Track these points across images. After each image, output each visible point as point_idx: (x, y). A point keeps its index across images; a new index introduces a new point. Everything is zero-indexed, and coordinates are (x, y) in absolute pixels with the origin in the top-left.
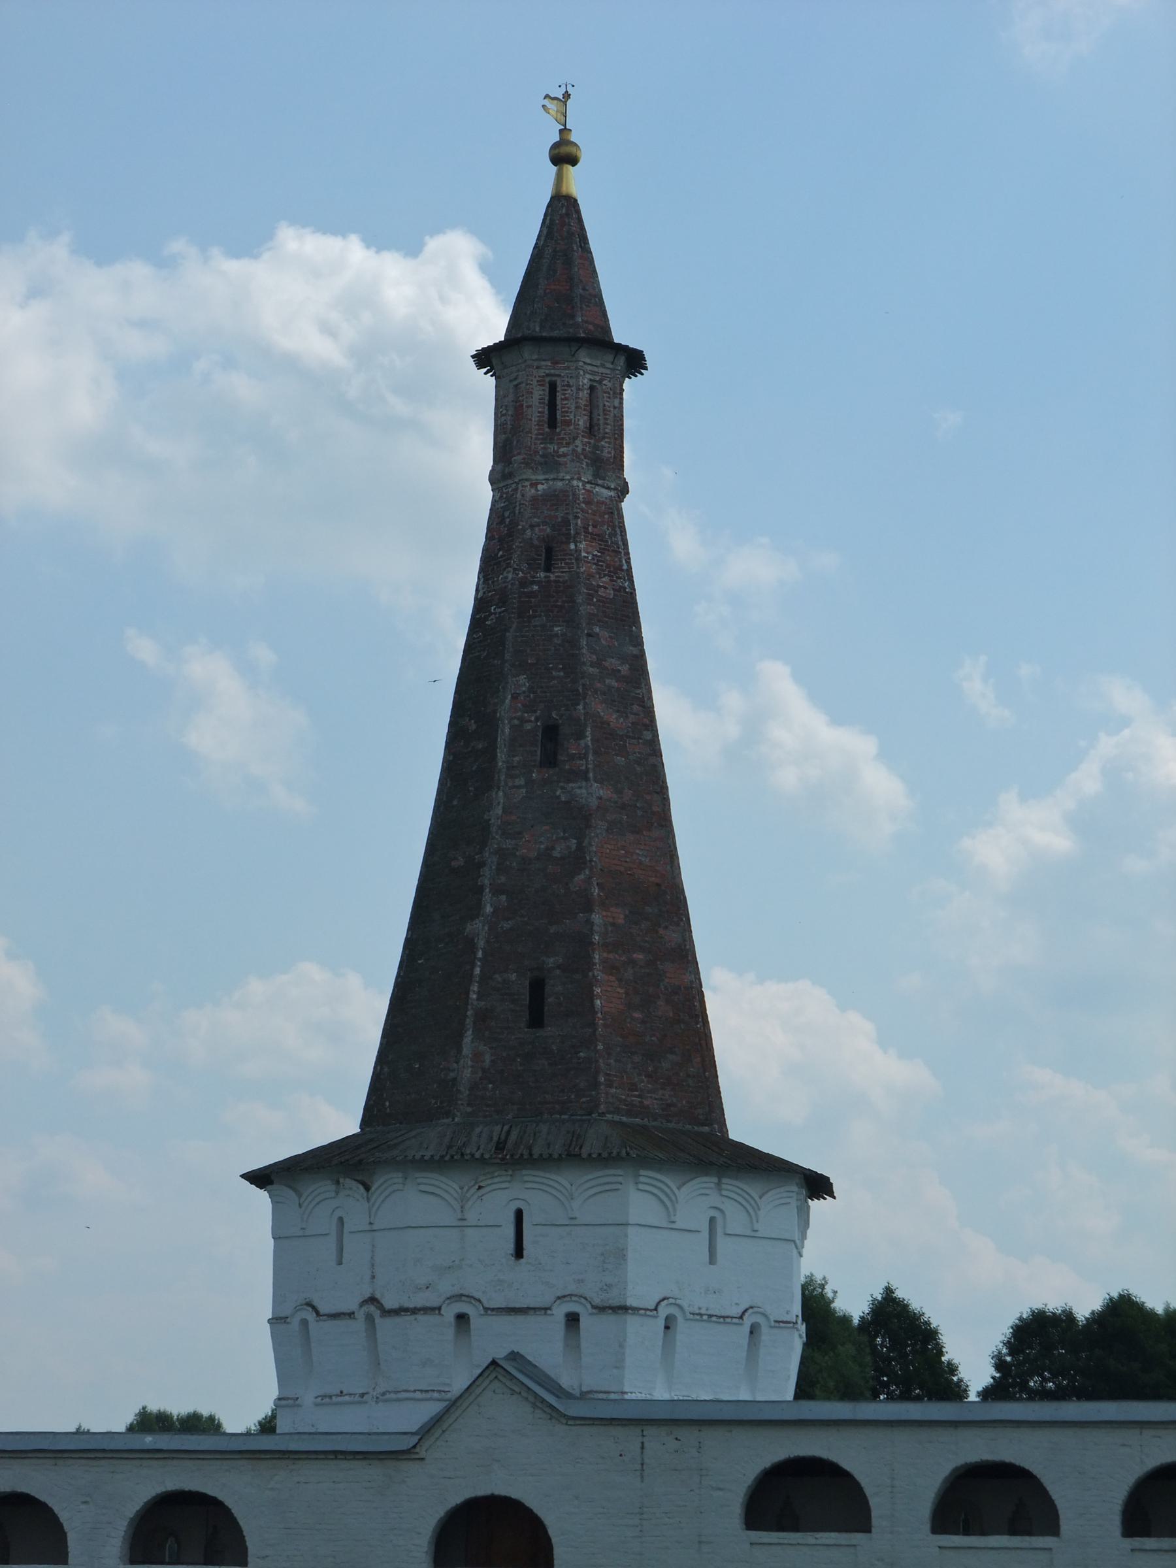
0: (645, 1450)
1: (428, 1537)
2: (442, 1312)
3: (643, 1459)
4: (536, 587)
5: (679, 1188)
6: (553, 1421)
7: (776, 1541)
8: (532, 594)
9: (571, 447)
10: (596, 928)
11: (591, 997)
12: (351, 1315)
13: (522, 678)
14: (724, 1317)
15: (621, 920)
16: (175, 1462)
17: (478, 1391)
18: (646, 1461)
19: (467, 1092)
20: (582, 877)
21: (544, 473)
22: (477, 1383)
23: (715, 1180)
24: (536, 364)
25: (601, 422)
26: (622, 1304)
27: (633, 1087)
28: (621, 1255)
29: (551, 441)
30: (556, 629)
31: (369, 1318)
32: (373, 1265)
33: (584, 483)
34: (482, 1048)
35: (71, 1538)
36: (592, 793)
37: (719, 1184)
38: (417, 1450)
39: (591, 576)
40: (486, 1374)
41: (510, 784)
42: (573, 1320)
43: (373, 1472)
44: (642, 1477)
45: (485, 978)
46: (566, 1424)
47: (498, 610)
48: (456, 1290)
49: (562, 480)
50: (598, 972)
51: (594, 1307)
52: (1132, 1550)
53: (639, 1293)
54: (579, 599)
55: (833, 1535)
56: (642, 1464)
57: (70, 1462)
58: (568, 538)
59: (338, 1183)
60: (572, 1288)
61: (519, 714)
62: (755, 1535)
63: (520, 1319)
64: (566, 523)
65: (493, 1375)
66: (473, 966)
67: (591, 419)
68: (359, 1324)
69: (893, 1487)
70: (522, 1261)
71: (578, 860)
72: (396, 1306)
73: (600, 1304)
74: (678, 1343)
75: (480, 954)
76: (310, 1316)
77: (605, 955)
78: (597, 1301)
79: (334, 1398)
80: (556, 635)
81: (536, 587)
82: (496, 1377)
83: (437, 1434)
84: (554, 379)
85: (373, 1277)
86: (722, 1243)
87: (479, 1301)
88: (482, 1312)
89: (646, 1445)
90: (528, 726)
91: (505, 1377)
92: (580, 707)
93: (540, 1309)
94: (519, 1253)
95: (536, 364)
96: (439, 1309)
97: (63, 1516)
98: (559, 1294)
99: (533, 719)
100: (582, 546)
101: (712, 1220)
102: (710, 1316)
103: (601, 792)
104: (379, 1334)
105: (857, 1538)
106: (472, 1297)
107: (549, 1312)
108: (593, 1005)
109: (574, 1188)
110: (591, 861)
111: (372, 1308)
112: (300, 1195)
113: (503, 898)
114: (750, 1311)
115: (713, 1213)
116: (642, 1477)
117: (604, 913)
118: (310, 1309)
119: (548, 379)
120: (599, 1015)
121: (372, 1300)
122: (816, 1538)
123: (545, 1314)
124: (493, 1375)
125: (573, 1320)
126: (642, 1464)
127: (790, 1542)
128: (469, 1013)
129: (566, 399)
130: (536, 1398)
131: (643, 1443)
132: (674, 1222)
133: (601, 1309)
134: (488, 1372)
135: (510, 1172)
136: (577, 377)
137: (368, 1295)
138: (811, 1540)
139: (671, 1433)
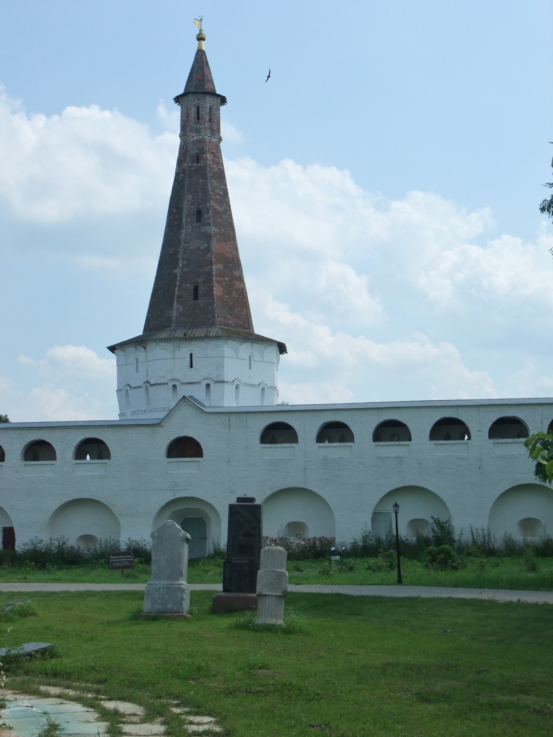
2: (169, 384)
4: (194, 168)
8: (193, 170)
11: (212, 290)
12: (141, 387)
13: (190, 196)
18: (231, 424)
20: (209, 255)
21: (196, 133)
22: (179, 403)
23: (251, 344)
27: (225, 318)
28: (222, 366)
31: (147, 388)
37: (252, 345)
38: (161, 423)
42: (208, 386)
44: (229, 429)
45: (180, 286)
47: (183, 175)
49: (201, 136)
56: (229, 426)
58: (204, 153)
60: (208, 376)
63: (192, 385)
64: (203, 148)
65: (184, 401)
66: (176, 282)
68: (143, 390)
71: (208, 250)
76: (128, 388)
77: (217, 278)
78: (215, 380)
81: (194, 168)
84: (199, 105)
86: (253, 363)
90: (192, 210)
92: (208, 204)
94: (191, 366)
96: (167, 383)
101: (250, 357)
102: (250, 384)
105: (294, 445)
106: (177, 380)
108: (213, 292)
110: (212, 250)
111: (147, 384)
112: (124, 352)
113: (185, 262)
120: (215, 296)
121: (147, 382)
124: (184, 401)
125: (208, 386)
126: (229, 426)
129: (202, 111)
131: (229, 419)
133: (217, 382)
134: (182, 400)
135: (188, 342)
136: (206, 104)
137: (146, 381)
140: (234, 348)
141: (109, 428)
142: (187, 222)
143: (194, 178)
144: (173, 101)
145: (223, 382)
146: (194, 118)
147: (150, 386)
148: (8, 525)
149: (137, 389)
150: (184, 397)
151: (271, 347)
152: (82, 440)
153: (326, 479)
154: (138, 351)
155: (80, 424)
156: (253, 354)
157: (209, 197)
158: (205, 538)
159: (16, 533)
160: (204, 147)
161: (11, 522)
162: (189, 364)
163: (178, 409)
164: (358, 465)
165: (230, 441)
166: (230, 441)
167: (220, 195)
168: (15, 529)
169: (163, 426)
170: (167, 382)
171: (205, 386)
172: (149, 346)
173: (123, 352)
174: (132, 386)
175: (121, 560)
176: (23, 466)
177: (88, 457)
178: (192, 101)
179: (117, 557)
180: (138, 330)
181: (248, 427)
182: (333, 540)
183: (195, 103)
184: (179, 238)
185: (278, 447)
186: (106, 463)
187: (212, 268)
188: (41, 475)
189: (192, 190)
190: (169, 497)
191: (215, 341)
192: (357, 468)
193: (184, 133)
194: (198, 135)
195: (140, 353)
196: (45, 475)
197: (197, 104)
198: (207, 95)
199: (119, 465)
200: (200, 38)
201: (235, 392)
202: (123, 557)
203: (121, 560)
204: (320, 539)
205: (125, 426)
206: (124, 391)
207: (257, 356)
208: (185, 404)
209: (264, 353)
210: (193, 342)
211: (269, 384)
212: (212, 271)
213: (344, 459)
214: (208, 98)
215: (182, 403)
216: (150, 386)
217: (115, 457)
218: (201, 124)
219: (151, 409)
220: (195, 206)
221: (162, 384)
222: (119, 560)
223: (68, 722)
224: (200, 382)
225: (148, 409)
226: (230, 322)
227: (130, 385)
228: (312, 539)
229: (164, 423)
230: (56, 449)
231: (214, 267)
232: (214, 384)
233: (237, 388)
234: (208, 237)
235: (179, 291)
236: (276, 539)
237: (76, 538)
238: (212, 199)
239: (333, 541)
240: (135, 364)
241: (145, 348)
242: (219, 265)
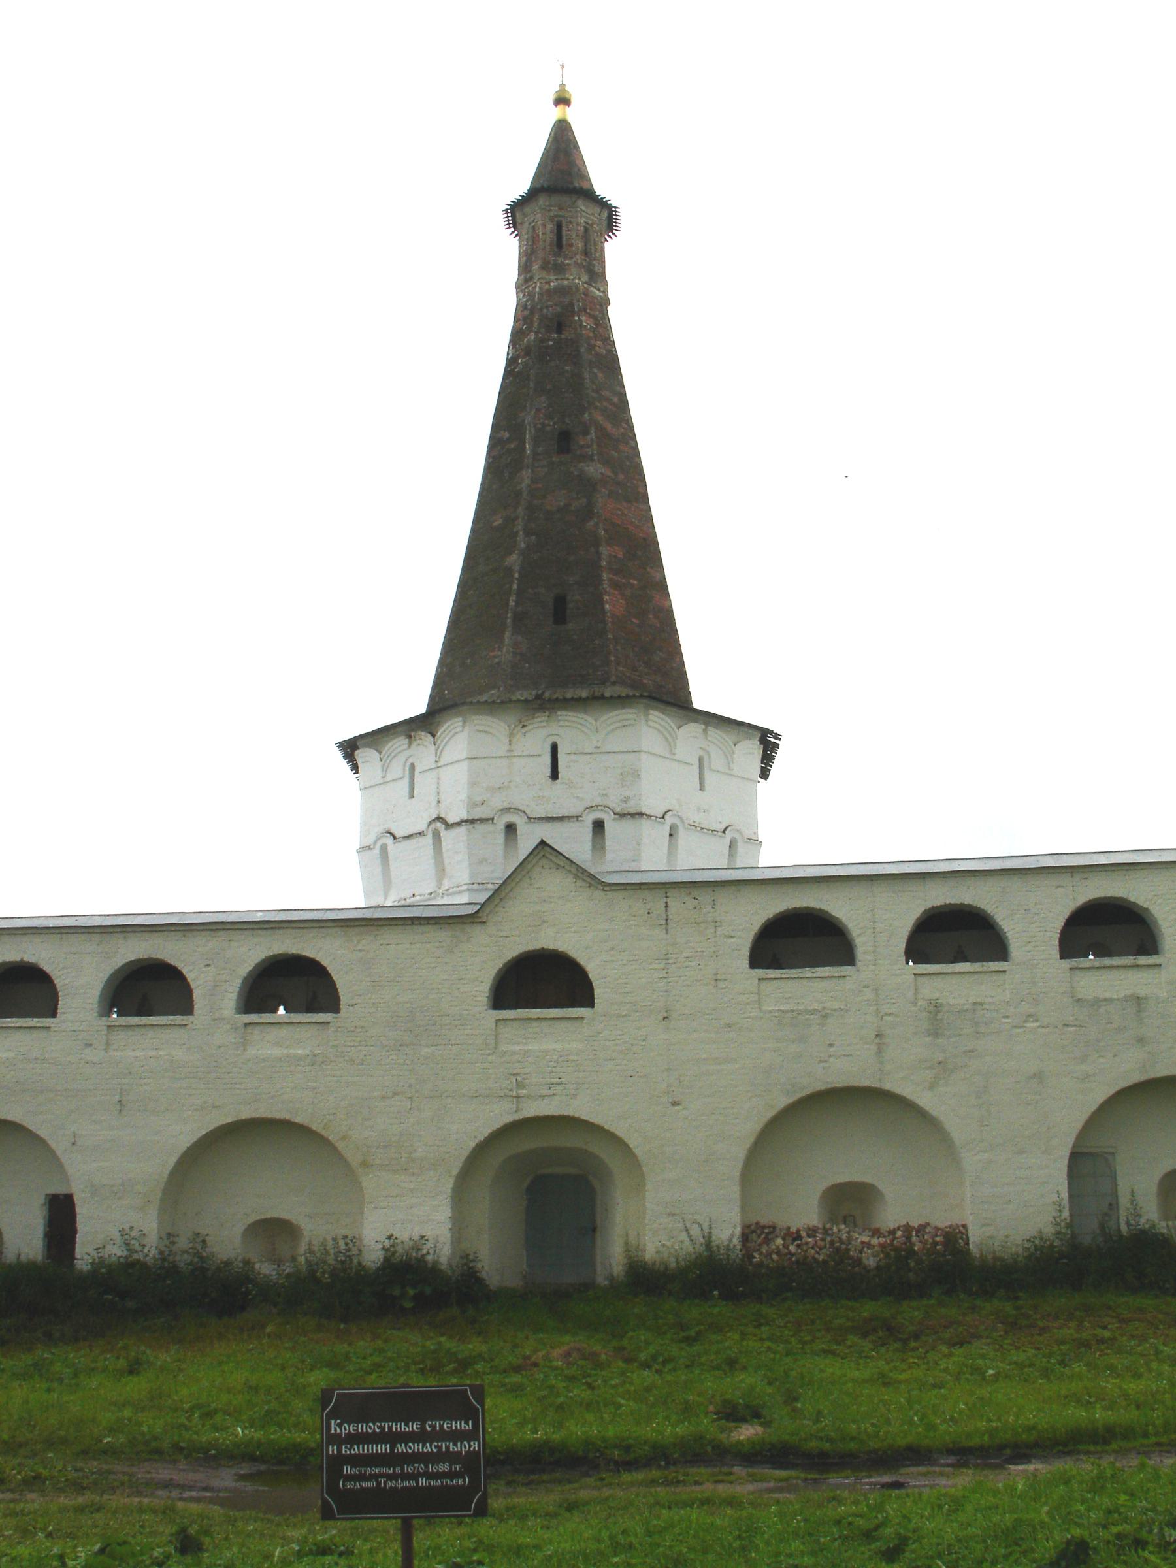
0: (668, 909)
1: (489, 985)
2: (495, 821)
3: (667, 916)
4: (551, 343)
5: (679, 728)
6: (592, 888)
7: (779, 976)
8: (547, 347)
9: (574, 259)
10: (604, 556)
11: (602, 603)
12: (421, 834)
13: (543, 399)
14: (712, 831)
15: (620, 555)
16: (281, 932)
17: (529, 866)
18: (670, 917)
19: (510, 670)
20: (592, 523)
22: (529, 859)
23: (703, 727)
24: (548, 208)
25: (593, 251)
26: (639, 811)
27: (634, 669)
28: (636, 774)
29: (559, 256)
30: (567, 368)
31: (437, 836)
32: (438, 793)
33: (583, 283)
34: (520, 638)
35: (197, 994)
36: (594, 470)
37: (705, 730)
38: (480, 915)
39: (589, 338)
40: (535, 853)
41: (536, 465)
42: (599, 826)
43: (442, 935)
44: (667, 930)
45: (520, 592)
46: (603, 890)
47: (524, 360)
48: (506, 805)
49: (568, 279)
50: (605, 585)
51: (615, 814)
52: (1071, 969)
53: (652, 803)
54: (582, 350)
55: (827, 968)
56: (667, 920)
57: (195, 933)
58: (573, 314)
59: (410, 737)
60: (598, 801)
61: (541, 421)
62: (760, 972)
63: (557, 824)
64: (571, 304)
65: (541, 854)
66: (511, 583)
67: (586, 245)
68: (428, 840)
69: (874, 928)
70: (557, 781)
71: (588, 512)
72: (457, 820)
73: (621, 812)
74: (679, 847)
75: (517, 575)
76: (389, 840)
77: (611, 576)
78: (618, 810)
79: (408, 900)
80: (567, 371)
81: (551, 343)
82: (543, 856)
83: (497, 901)
84: (560, 218)
85: (439, 802)
86: (707, 775)
87: (524, 812)
88: (527, 821)
89: (669, 904)
90: (548, 428)
91: (551, 854)
92: (586, 415)
93: (572, 817)
94: (555, 775)
95: (548, 208)
96: (493, 819)
97: (190, 977)
98: (588, 805)
99: (551, 423)
100: (584, 318)
101: (701, 760)
102: (702, 828)
103: (603, 471)
104: (444, 844)
105: (847, 970)
106: (518, 810)
107: (580, 819)
108: (603, 608)
109: (598, 723)
110: (598, 513)
111: (439, 824)
112: (380, 753)
113: (533, 538)
114: (730, 828)
115: (701, 753)
116: (667, 930)
117: (608, 548)
118: (389, 835)
119: (556, 219)
120: (608, 614)
121: (439, 819)
122: (813, 972)
123: (577, 820)
124: (541, 854)
125: (599, 826)
126: (667, 920)
127: (792, 976)
128: (509, 615)
129: (569, 231)
130: (577, 870)
131: (666, 903)
132: (674, 754)
133: (622, 815)
134: (537, 851)
135: (547, 713)
136: (577, 217)
137: (434, 816)
138: (809, 974)
139: (690, 894)
140: (665, 733)
141: (337, 929)
142: (535, 454)
143: (553, 364)
144: (500, 220)
145: (641, 814)
146: (551, 245)
147: (446, 829)
148: (60, 1190)
149: (414, 841)
150: (543, 843)
151: (748, 742)
152: (263, 961)
153: (940, 1063)
154: (415, 744)
155: (259, 917)
156: (708, 752)
157: (588, 402)
158: (594, 1230)
159: (80, 1210)
160: (575, 301)
161: (65, 1178)
162: (548, 771)
163: (524, 876)
164: (1025, 1021)
165: (670, 961)
166: (670, 961)
167: (614, 404)
168: (76, 1199)
169: (484, 922)
170: (491, 817)
171: (591, 826)
172: (447, 724)
173: (377, 753)
174: (399, 833)
175: (401, 1448)
176: (105, 1028)
177: (281, 1011)
178: (536, 215)
179: (372, 1427)
180: (418, 706)
181: (718, 924)
182: (960, 1232)
183: (552, 214)
184: (518, 488)
185: (800, 975)
186: (329, 1023)
187: (598, 552)
188: (153, 1053)
189: (549, 387)
190: (501, 1114)
191: (617, 712)
192: (1023, 1030)
193: (528, 276)
194: (559, 277)
195: (423, 751)
196: (161, 1053)
197: (556, 216)
198: (578, 198)
199: (362, 1027)
200: (562, 100)
201: (666, 844)
202: (415, 1427)
203: (401, 1448)
204: (921, 1229)
205: (380, 923)
206: (377, 851)
207: (717, 760)
208: (544, 862)
209: (733, 753)
210: (559, 713)
211: (748, 833)
212: (600, 559)
213: (987, 1007)
214: (581, 204)
215: (535, 861)
216: (446, 829)
217: (352, 1006)
218: (566, 257)
219: (447, 887)
220: (556, 419)
221: (477, 820)
222: (383, 1448)
223: (563, 66)
224: (577, 817)
225: (440, 888)
226: (645, 681)
227: (392, 832)
228: (898, 1229)
229: (487, 916)
230: (192, 985)
231: (604, 550)
232: (614, 819)
233: (671, 835)
234: (588, 486)
235: (517, 603)
236: (798, 1231)
237: (239, 1229)
238: (596, 407)
239: (959, 1236)
240: (406, 780)
241: (434, 736)
242: (615, 547)
